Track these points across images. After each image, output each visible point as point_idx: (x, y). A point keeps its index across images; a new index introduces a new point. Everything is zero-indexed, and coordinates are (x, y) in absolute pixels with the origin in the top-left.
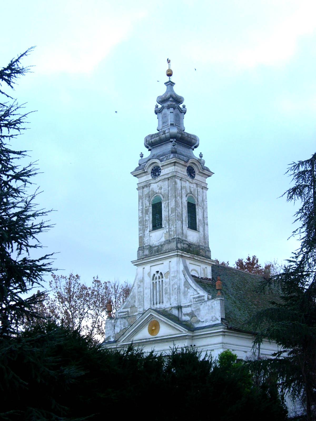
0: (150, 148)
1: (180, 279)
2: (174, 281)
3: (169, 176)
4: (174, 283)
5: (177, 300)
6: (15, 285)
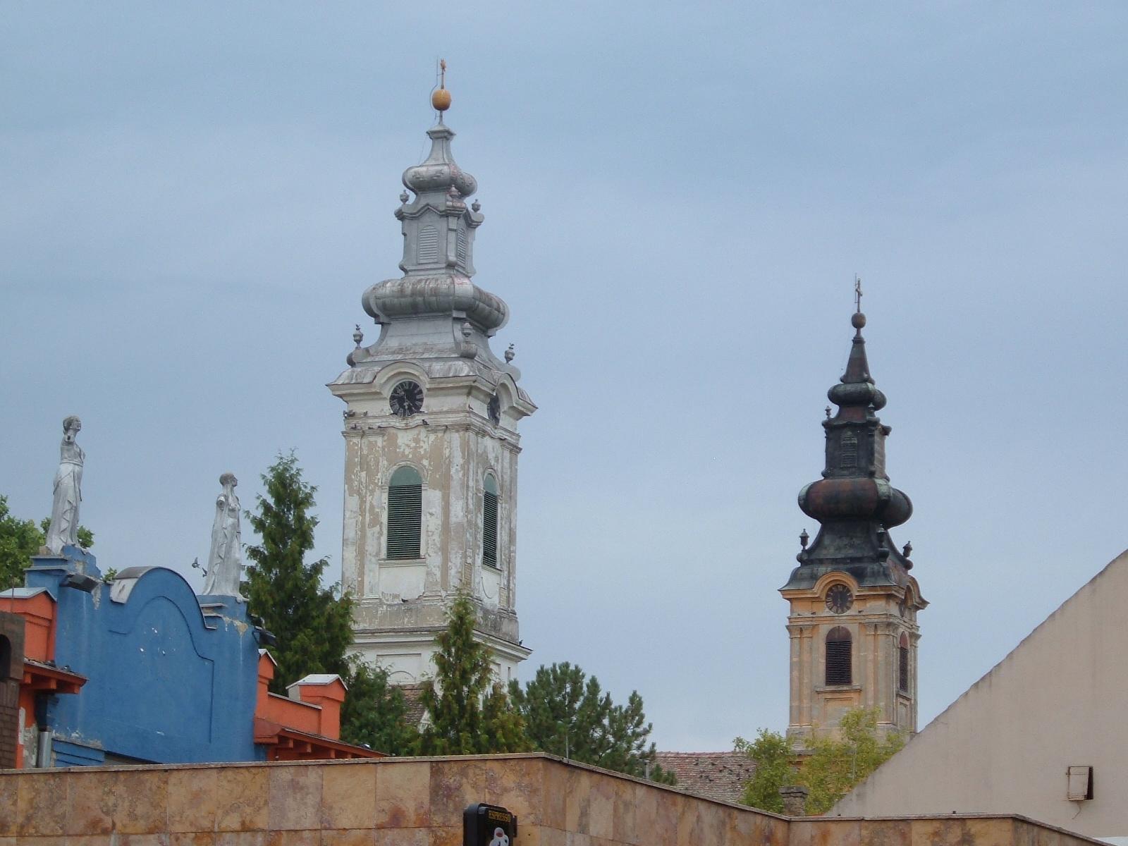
0: (383, 318)
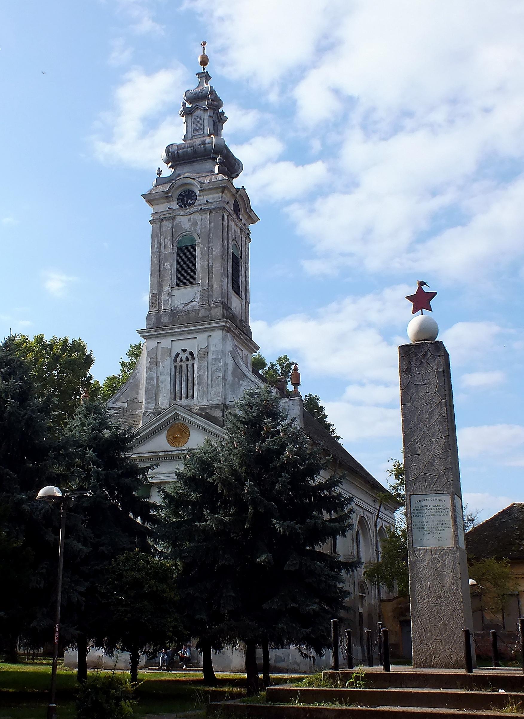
1: (226, 364)
2: (216, 366)
3: (213, 207)
4: (217, 369)
5: (221, 394)
6: (314, 480)
